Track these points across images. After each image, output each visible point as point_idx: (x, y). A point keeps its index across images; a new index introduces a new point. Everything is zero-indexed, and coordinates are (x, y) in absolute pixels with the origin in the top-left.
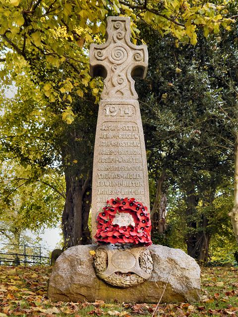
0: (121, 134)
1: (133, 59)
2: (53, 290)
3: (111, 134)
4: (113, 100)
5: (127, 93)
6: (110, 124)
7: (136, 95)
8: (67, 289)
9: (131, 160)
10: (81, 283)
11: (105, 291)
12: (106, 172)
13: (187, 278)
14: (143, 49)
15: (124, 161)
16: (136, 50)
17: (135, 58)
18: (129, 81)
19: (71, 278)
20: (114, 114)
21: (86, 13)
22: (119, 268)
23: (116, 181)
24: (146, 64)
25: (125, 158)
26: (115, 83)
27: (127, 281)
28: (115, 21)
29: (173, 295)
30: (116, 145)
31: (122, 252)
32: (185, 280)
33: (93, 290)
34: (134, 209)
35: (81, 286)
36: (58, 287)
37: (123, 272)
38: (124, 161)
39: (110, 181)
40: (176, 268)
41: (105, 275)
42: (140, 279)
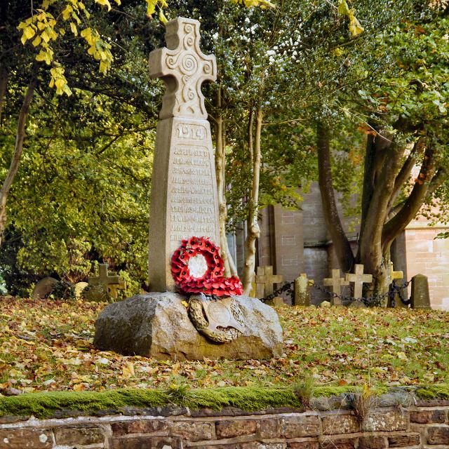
0: (193, 159)
1: (183, 32)
2: (156, 348)
3: (184, 159)
4: (186, 120)
5: (197, 111)
6: (182, 148)
7: (206, 115)
8: (173, 348)
9: (203, 191)
10: (186, 339)
11: (203, 348)
12: (179, 205)
13: (272, 332)
14: (195, 25)
15: (196, 192)
16: (205, 60)
17: (204, 70)
18: (199, 97)
19: (176, 335)
20: (188, 136)
21: (343, 400)
22: (219, 322)
23: (189, 215)
24: (214, 78)
25: (198, 188)
26: (186, 98)
27: (229, 336)
28: (186, 23)
29: (262, 351)
30: (189, 173)
31: (215, 304)
32: (271, 333)
33: (195, 347)
34: (209, 250)
35: (185, 342)
36: (162, 345)
37: (224, 326)
38: (196, 192)
39: (184, 214)
40: (262, 320)
41: (211, 330)
42: (239, 334)
